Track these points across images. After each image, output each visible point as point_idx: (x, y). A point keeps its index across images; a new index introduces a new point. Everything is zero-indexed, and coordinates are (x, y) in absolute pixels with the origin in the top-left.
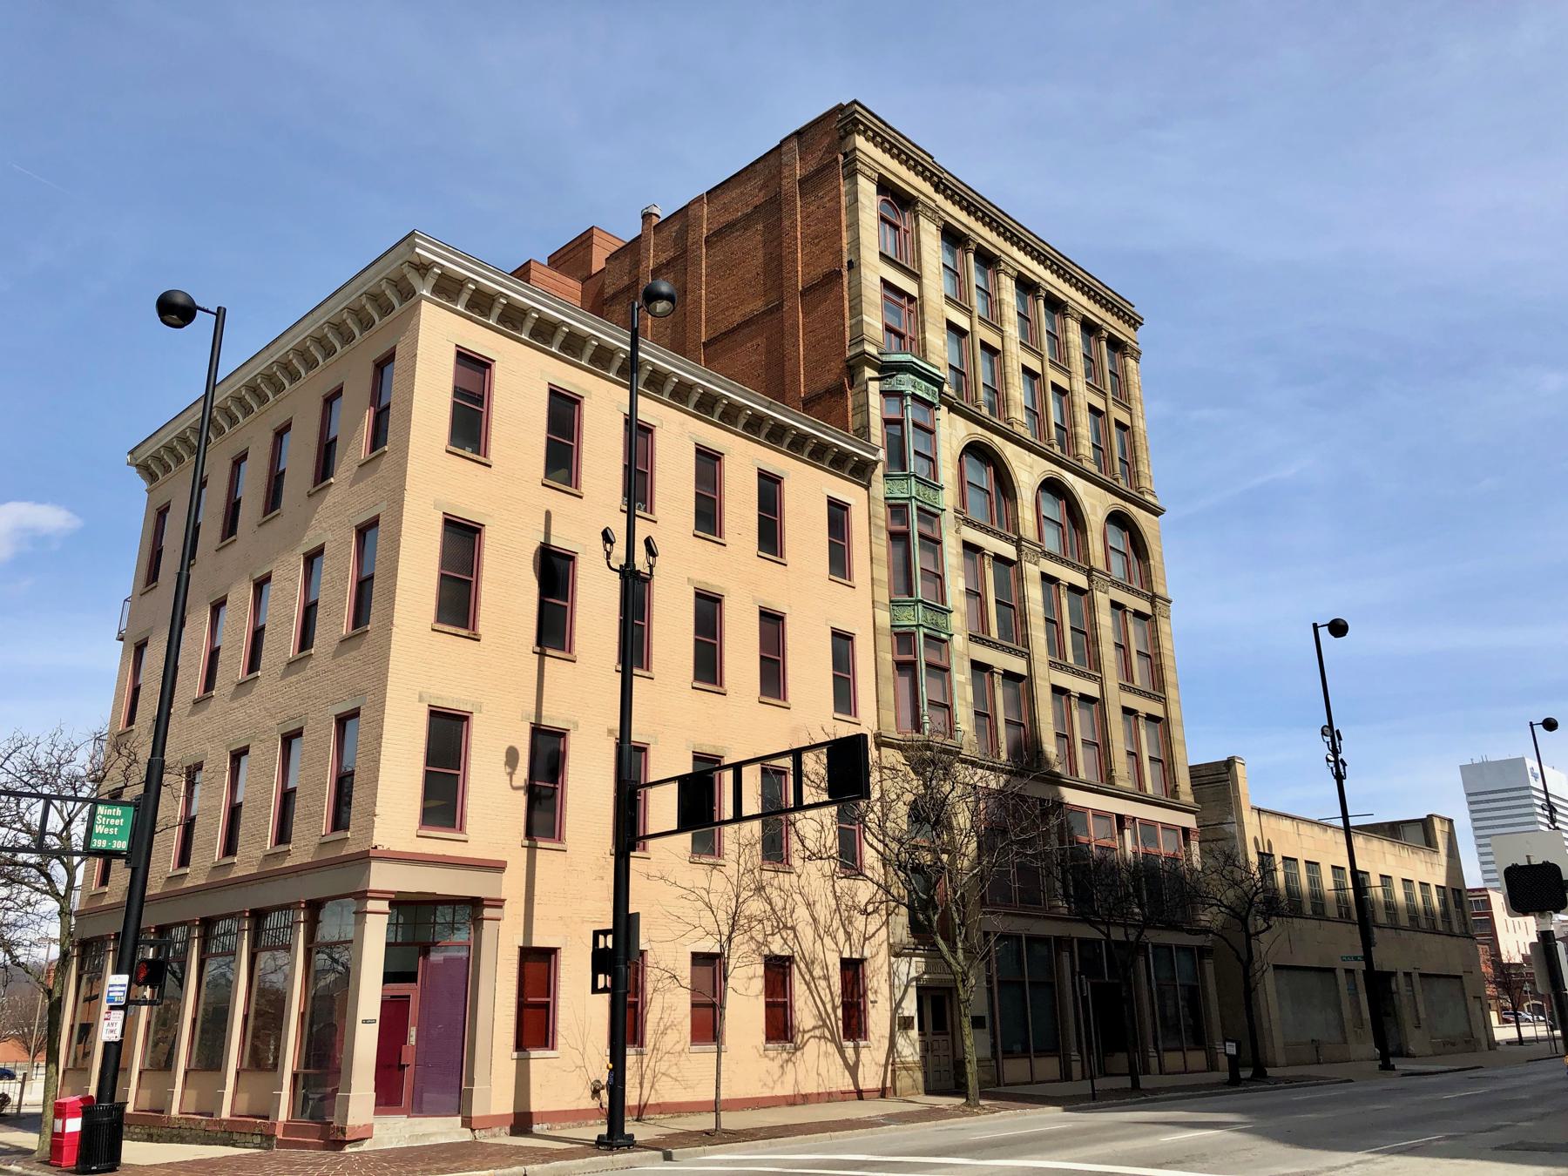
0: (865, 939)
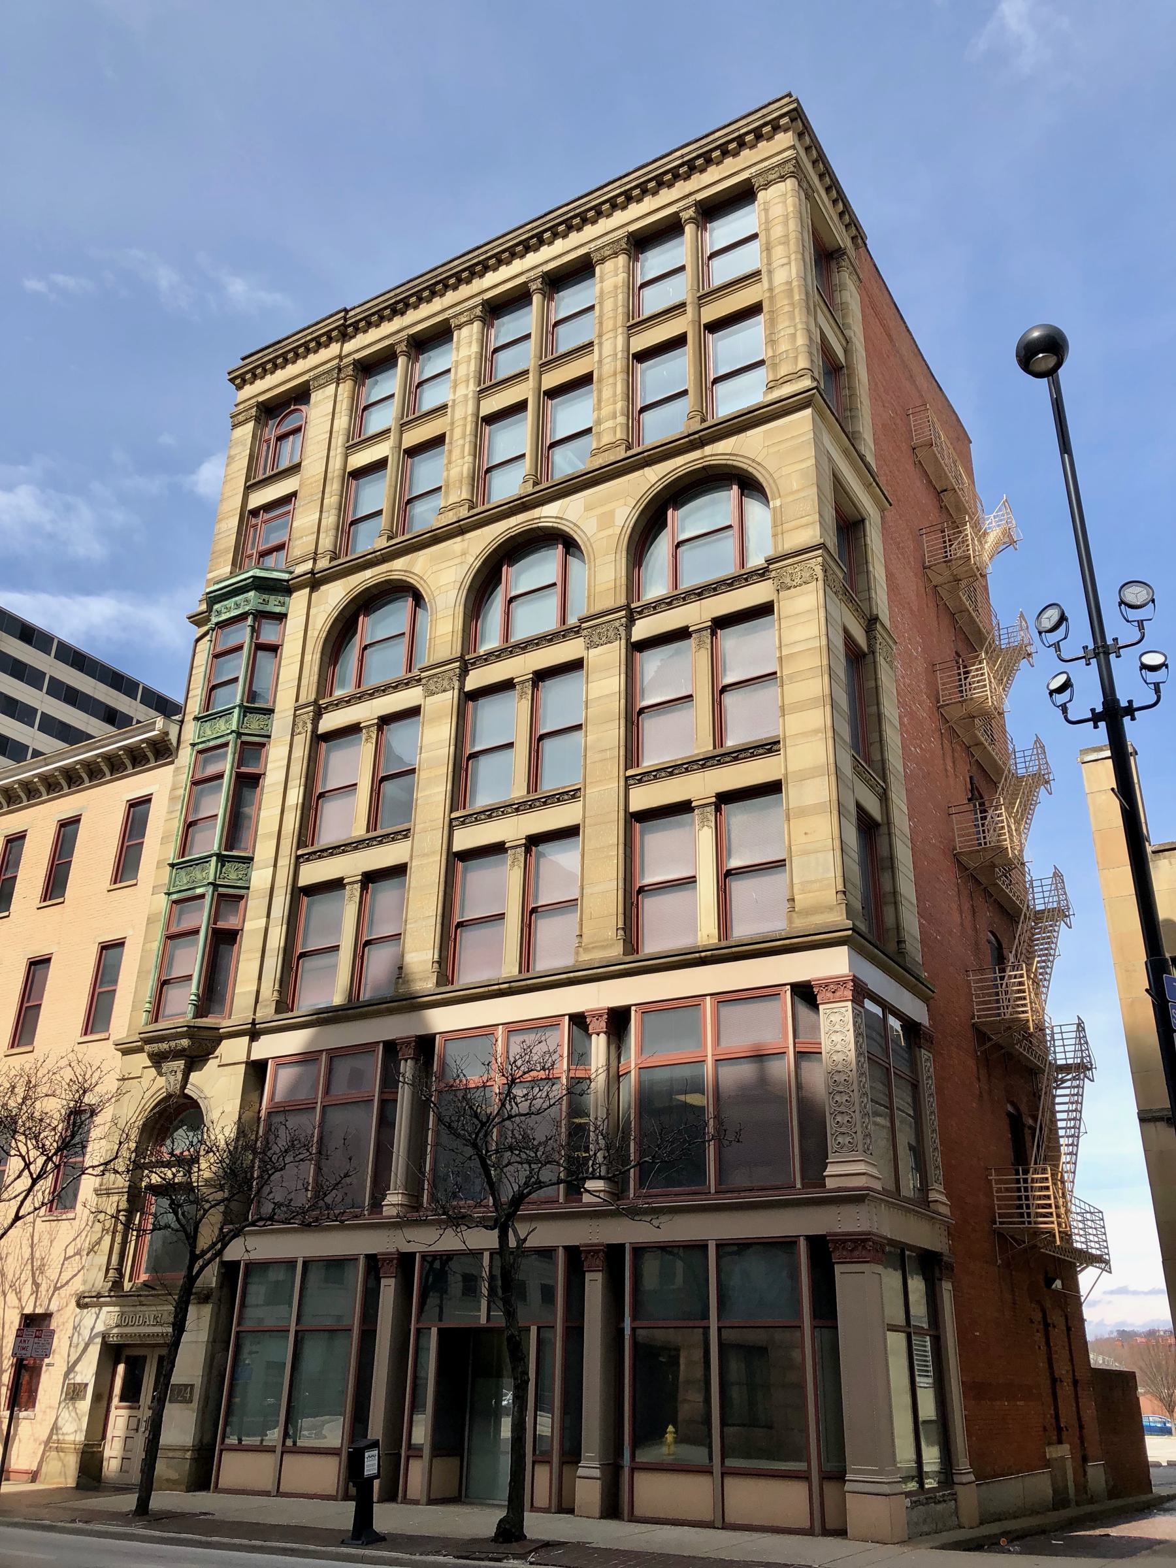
0: (56, 1289)
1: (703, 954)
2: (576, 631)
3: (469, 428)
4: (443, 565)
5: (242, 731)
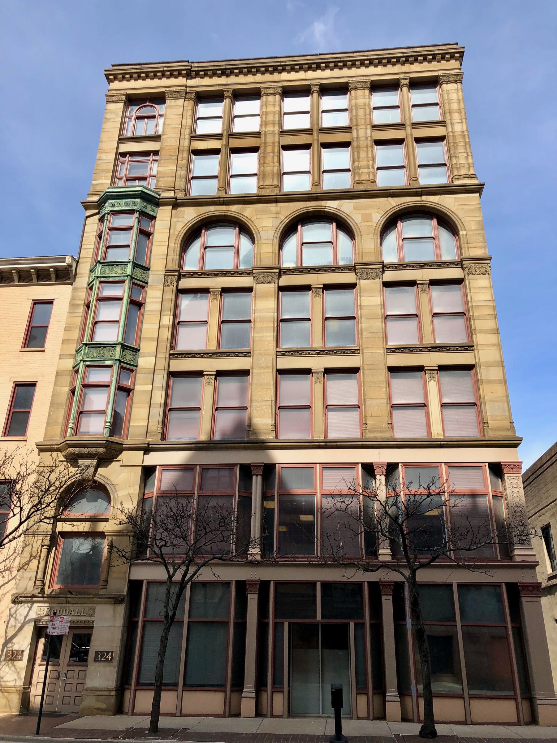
1: (442, 443)
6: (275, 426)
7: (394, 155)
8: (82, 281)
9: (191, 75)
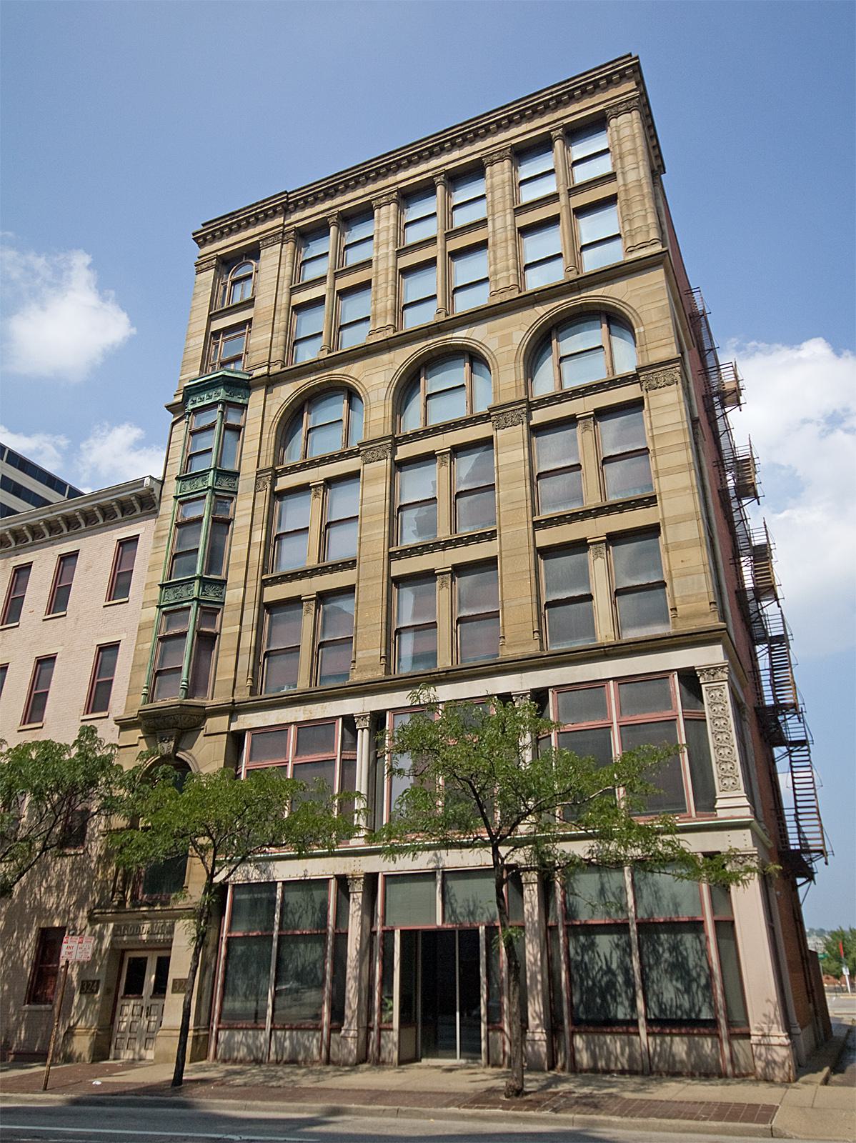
2: (355, 453)
3: (391, 276)
4: (374, 371)
5: (216, 487)
6: (387, 657)
7: (550, 242)
8: (168, 507)
9: (289, 210)
